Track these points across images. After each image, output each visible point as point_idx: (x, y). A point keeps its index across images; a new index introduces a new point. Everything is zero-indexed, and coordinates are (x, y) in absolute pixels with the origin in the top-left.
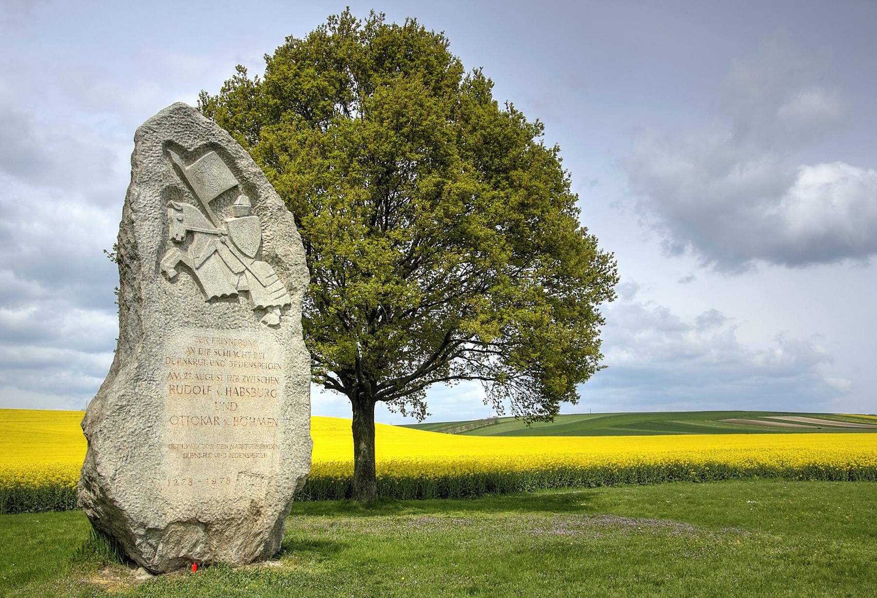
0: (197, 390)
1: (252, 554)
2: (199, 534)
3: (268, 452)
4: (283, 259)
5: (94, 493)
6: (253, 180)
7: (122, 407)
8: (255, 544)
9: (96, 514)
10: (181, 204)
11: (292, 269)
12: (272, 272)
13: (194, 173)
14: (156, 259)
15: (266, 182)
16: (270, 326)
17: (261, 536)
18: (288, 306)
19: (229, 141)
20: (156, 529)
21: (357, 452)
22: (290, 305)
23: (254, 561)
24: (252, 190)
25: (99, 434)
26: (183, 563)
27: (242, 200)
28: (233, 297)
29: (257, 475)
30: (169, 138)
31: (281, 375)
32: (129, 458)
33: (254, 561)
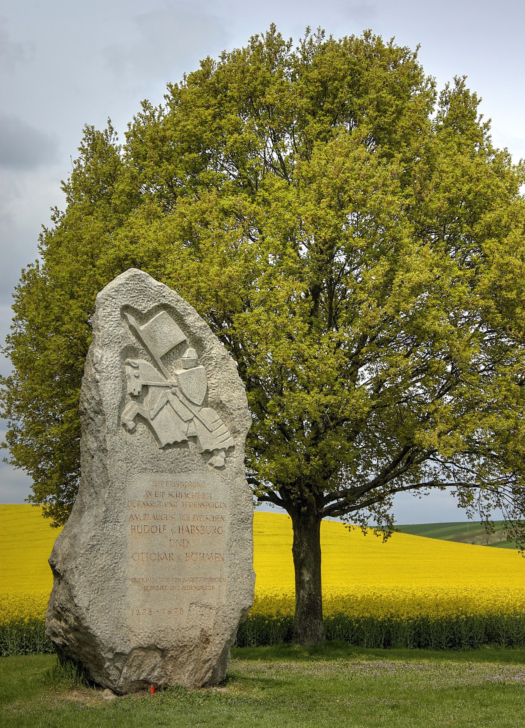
0: (154, 529)
1: (202, 679)
2: (156, 659)
3: (216, 585)
4: (227, 405)
5: (66, 621)
6: (200, 334)
7: (93, 546)
8: (204, 670)
9: (65, 641)
10: (137, 361)
11: (236, 413)
12: (217, 417)
13: (147, 331)
14: (117, 414)
15: (211, 334)
16: (216, 467)
17: (210, 663)
18: (232, 448)
19: (178, 301)
20: (121, 654)
21: (299, 583)
22: (234, 447)
23: (203, 686)
24: (198, 343)
25: (75, 570)
26: (143, 685)
27: (190, 353)
28: (184, 443)
29: (206, 606)
30: (126, 303)
31: (227, 513)
32: (100, 591)
33: (203, 686)
